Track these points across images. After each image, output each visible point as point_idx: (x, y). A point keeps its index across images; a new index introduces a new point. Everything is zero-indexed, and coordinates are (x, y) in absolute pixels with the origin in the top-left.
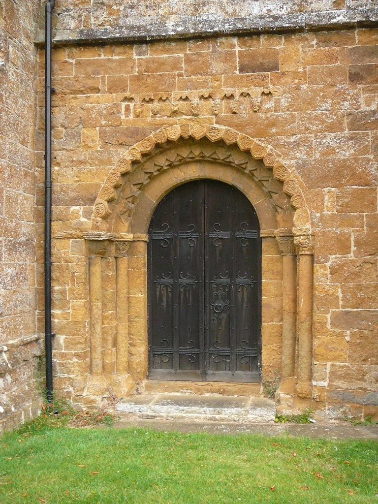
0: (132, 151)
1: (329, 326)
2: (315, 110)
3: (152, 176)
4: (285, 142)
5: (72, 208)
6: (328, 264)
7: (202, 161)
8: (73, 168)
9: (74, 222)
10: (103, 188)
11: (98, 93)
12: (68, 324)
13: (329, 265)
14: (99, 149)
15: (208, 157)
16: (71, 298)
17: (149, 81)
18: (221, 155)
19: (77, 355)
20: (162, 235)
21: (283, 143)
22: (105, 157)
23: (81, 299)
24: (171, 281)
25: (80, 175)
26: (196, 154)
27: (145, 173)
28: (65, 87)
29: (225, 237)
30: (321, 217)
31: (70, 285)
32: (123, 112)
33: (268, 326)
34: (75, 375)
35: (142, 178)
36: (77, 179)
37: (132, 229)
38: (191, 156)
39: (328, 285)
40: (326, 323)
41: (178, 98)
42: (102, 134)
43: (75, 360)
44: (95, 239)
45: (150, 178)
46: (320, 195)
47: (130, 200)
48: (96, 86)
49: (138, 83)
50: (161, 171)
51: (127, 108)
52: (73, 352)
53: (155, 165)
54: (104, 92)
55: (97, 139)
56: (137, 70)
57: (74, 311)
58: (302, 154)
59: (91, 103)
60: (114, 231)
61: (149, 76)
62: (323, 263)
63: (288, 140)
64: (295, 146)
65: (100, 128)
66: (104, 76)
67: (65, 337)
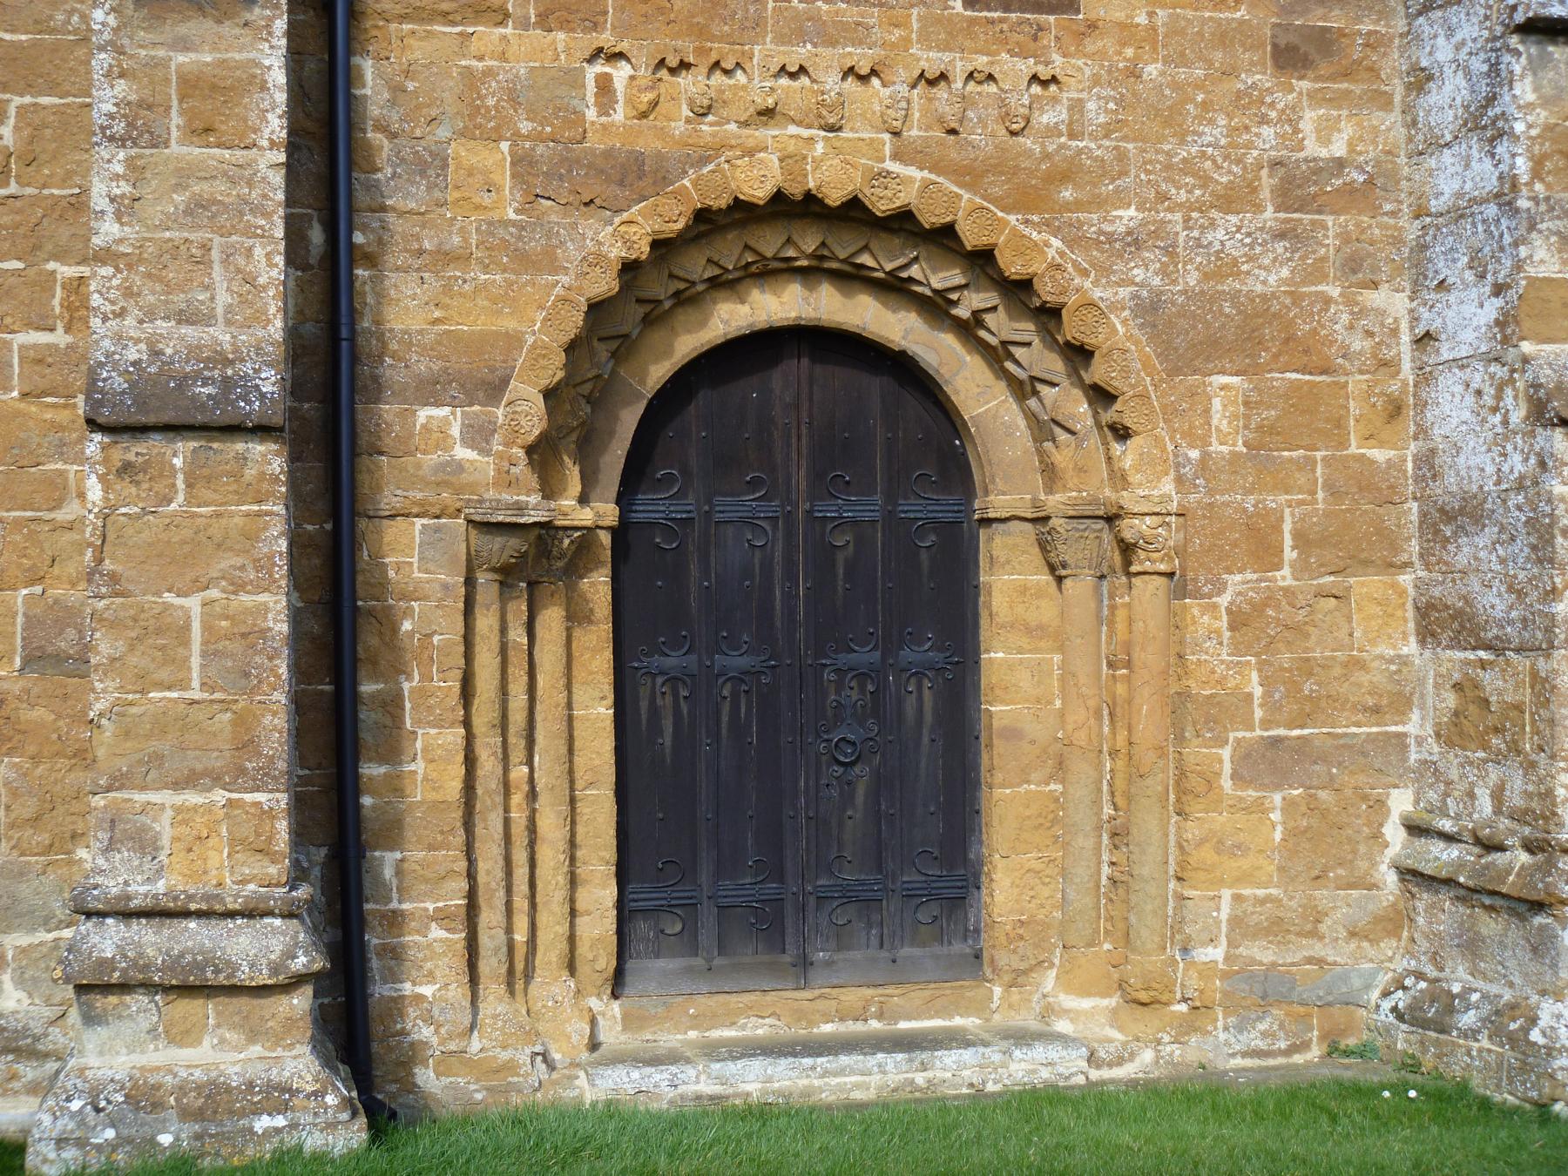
0: (623, 228)
1: (1227, 784)
2: (1183, 142)
4: (1101, 232)
5: (424, 414)
6: (1224, 600)
9: (433, 459)
10: (534, 347)
11: (500, 24)
14: (512, 216)
15: (844, 261)
16: (417, 722)
22: (535, 244)
32: (591, 99)
33: (1010, 800)
36: (437, 314)
39: (1222, 662)
41: (775, 68)
42: (523, 164)
44: (508, 520)
46: (1198, 396)
52: (431, 906)
53: (671, 276)
57: (432, 766)
59: (481, 58)
64: (1129, 245)
65: (514, 144)
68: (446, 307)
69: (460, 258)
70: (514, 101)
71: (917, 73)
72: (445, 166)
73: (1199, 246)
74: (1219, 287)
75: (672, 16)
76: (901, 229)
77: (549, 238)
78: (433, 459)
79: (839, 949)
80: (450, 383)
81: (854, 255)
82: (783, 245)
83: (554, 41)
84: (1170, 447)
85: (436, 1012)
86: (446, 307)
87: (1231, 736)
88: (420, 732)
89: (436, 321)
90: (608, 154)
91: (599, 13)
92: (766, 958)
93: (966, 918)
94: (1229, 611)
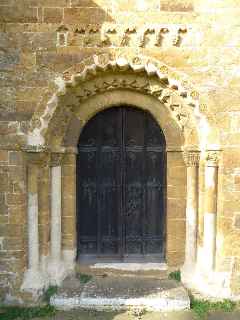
0: (65, 74)
1: (233, 226)
2: (224, 46)
3: (82, 100)
4: (199, 72)
5: (11, 123)
6: (233, 175)
7: (123, 88)
8: (13, 87)
9: (12, 135)
10: (40, 105)
11: (36, 22)
12: (7, 226)
13: (234, 176)
14: (36, 71)
15: (130, 85)
16: (9, 204)
17: (81, 14)
18: (140, 83)
19: (14, 254)
20: (88, 148)
21: (197, 73)
22: (41, 79)
23: (18, 204)
24: (95, 185)
25: (18, 94)
26: (119, 82)
27: (77, 96)
28: (5, 15)
29: (139, 151)
30: (228, 137)
31: (8, 192)
32: (58, 41)
34: (13, 272)
35: (74, 101)
36: (15, 97)
37: (65, 143)
38: (115, 84)
39: (233, 192)
40: (231, 224)
41: (107, 30)
42: (39, 59)
43: (13, 258)
44: (32, 151)
45: (80, 101)
47: (64, 118)
48: (33, 16)
49: (72, 16)
50: (90, 96)
51: (62, 37)
52: (11, 251)
53: (85, 90)
54: (41, 22)
55: (35, 62)
56: (71, 4)
57: (12, 215)
58: (212, 82)
59: (29, 31)
60: (49, 145)
61: (81, 9)
62: (229, 173)
63: (201, 70)
64: (207, 75)
65: (37, 53)
66: (41, 8)
67: (3, 238)
68: (17, 96)
69: (22, 83)
70: (37, 42)
71: (146, 30)
72: (18, 59)
73: (228, 75)
74: (234, 86)
75: (80, 18)
76: (144, 76)
77: (45, 77)
78: (12, 135)
79: (131, 254)
80: (17, 115)
81: (132, 84)
82: (113, 82)
83: (48, 26)
84: (218, 132)
85: (12, 278)
86: (17, 96)
87: (235, 213)
88: (9, 206)
89: (15, 99)
90: (62, 55)
91: (60, 18)
92: (113, 255)
93: (162, 248)
94: (235, 178)
